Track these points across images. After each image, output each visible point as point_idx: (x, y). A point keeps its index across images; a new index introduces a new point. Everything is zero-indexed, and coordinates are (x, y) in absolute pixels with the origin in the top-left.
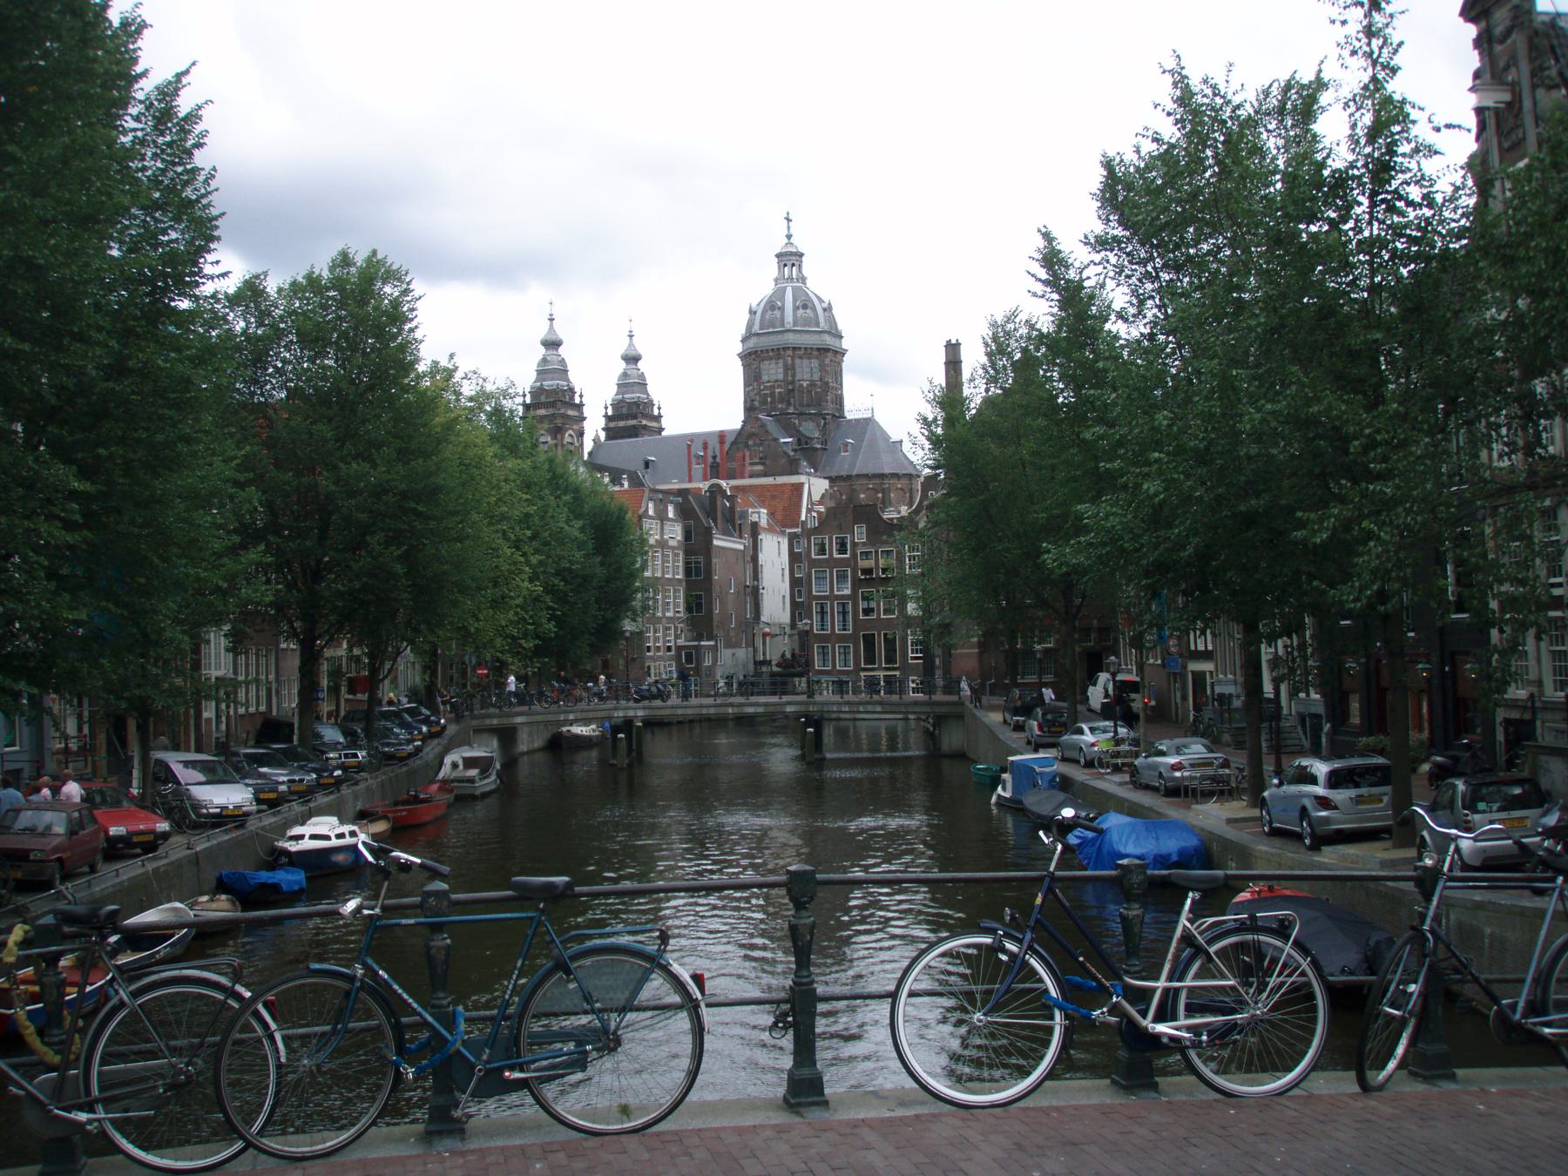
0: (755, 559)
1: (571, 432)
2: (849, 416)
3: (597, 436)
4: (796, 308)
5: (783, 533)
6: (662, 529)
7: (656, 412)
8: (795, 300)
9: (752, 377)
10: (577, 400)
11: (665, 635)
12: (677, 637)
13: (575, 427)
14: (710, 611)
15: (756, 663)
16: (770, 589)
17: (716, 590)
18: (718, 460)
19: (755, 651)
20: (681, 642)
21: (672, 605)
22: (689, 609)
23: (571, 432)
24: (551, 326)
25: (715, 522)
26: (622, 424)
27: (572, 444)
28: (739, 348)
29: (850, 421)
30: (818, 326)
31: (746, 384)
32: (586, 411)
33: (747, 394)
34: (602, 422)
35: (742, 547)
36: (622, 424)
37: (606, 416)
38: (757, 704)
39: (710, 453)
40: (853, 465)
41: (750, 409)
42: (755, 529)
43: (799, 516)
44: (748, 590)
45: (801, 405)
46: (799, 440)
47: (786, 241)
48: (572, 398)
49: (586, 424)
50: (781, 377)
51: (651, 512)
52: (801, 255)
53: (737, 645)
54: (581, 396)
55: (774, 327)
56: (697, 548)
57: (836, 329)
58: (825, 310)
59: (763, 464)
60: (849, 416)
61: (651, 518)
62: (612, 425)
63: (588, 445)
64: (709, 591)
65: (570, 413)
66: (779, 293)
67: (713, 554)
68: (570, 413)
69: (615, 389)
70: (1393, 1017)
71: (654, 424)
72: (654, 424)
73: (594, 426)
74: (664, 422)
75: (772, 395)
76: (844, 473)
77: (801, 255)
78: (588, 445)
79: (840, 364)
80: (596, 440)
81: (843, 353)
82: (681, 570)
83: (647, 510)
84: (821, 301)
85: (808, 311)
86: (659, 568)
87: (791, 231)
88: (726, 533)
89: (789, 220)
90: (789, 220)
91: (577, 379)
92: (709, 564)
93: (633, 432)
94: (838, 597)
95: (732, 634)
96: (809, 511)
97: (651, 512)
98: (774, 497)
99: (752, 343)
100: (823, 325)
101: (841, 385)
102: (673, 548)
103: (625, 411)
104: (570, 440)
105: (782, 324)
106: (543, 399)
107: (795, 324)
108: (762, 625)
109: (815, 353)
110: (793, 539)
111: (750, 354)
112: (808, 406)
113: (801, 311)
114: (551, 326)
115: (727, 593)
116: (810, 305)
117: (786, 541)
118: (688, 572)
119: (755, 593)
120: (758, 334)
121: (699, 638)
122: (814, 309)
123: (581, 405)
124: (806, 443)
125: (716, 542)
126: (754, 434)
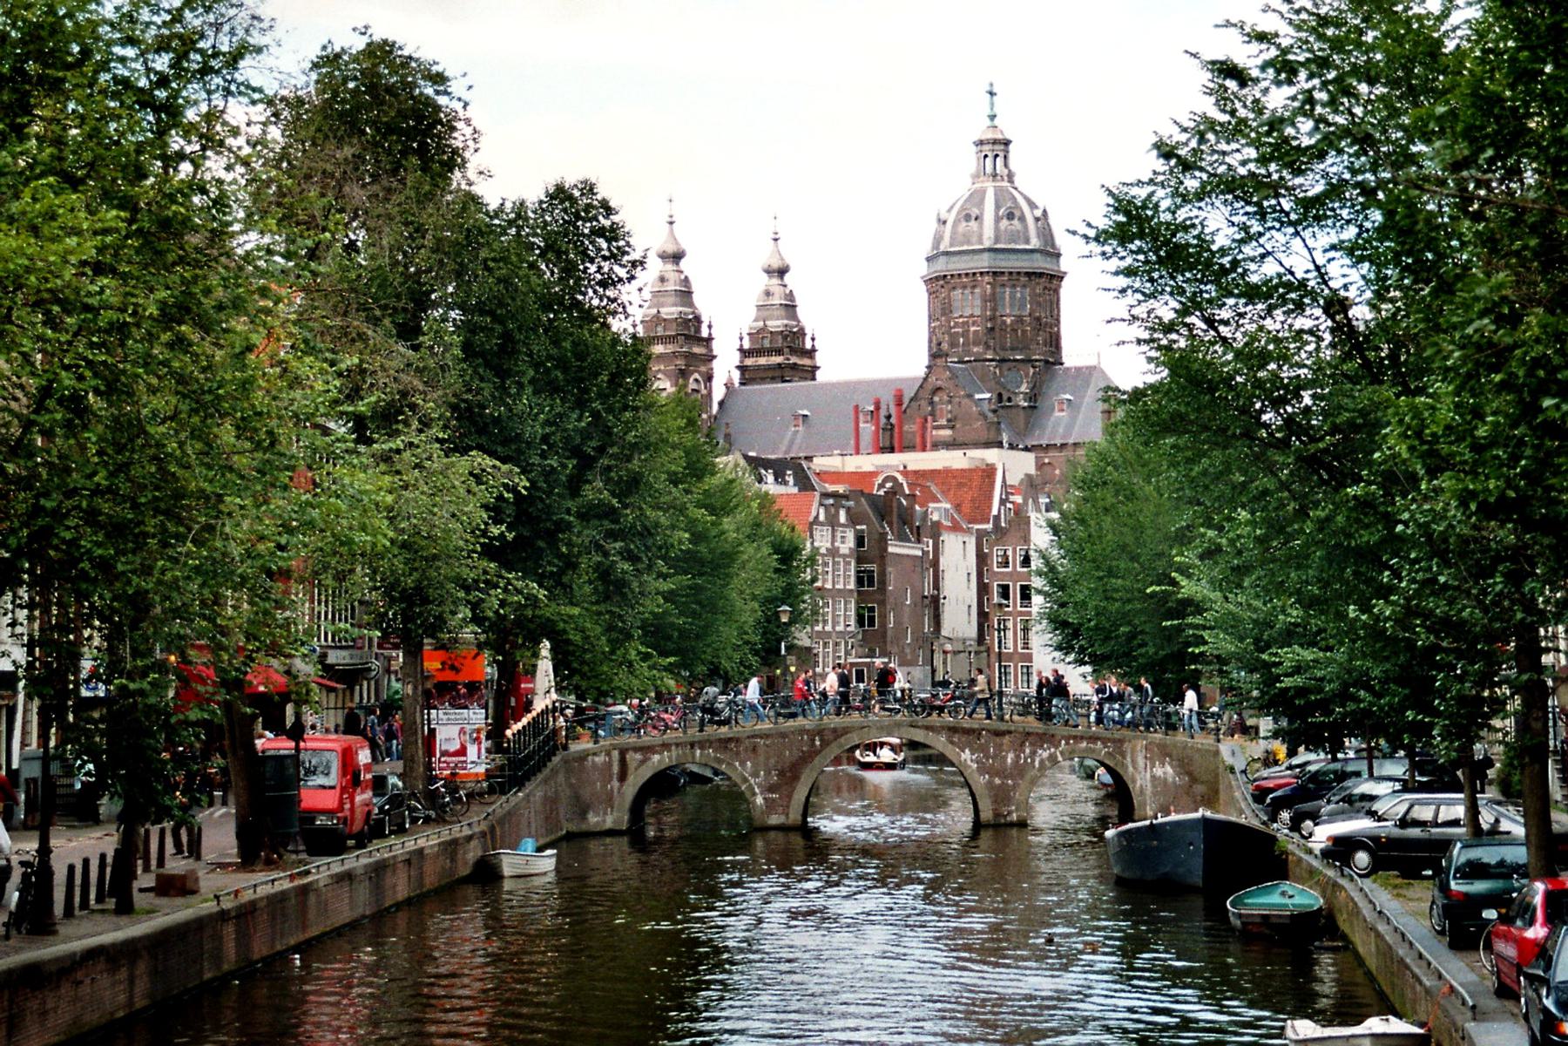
0: (935, 564)
1: (696, 376)
2: (1067, 364)
3: (730, 379)
4: (998, 219)
5: (969, 531)
6: (833, 536)
7: (808, 345)
8: (998, 207)
9: (940, 311)
10: (705, 333)
11: (835, 651)
12: (847, 653)
13: (703, 369)
14: (883, 625)
15: (935, 684)
16: (953, 602)
17: (891, 600)
18: (893, 420)
19: (934, 671)
20: (851, 660)
21: (841, 617)
22: (860, 620)
23: (696, 376)
24: (672, 231)
25: (890, 524)
26: (762, 361)
27: (697, 391)
28: (923, 269)
29: (1068, 369)
30: (1027, 241)
31: (931, 318)
32: (717, 347)
33: (932, 332)
34: (736, 358)
35: (919, 553)
36: (762, 361)
37: (741, 350)
38: (334, 970)
39: (883, 413)
40: (1070, 427)
41: (936, 355)
42: (936, 530)
43: (990, 507)
44: (927, 601)
45: (1004, 349)
46: (1000, 395)
47: (988, 123)
48: (698, 330)
49: (715, 364)
50: (977, 312)
51: (822, 518)
52: (1007, 143)
53: (913, 663)
54: (710, 327)
55: (969, 243)
56: (870, 556)
57: (1053, 245)
58: (1037, 219)
59: (953, 428)
60: (1067, 364)
61: (822, 524)
62: (749, 362)
63: (718, 393)
64: (882, 603)
65: (697, 350)
66: (977, 197)
67: (888, 560)
68: (697, 350)
69: (753, 312)
70: (779, 650)
71: (806, 362)
72: (806, 362)
73: (726, 367)
74: (819, 359)
75: (965, 334)
76: (1058, 442)
77: (1007, 143)
78: (718, 393)
79: (1056, 291)
80: (729, 386)
81: (1060, 277)
82: (853, 580)
83: (817, 517)
84: (1032, 205)
85: (1016, 222)
86: (830, 577)
87: (996, 110)
88: (902, 537)
89: (992, 94)
90: (992, 94)
91: (704, 303)
92: (883, 573)
93: (780, 374)
94: (1021, 614)
95: (908, 650)
96: (1003, 502)
97: (822, 518)
98: (960, 485)
99: (941, 266)
100: (1035, 243)
101: (1058, 320)
102: (844, 556)
103: (767, 344)
104: (695, 386)
105: (980, 241)
106: (660, 331)
107: (997, 240)
108: (942, 640)
109: (1023, 279)
110: (980, 536)
111: (937, 278)
112: (1012, 349)
113: (1004, 223)
114: (672, 231)
115: (903, 604)
116: (1017, 214)
117: (973, 540)
118: (860, 581)
119: (935, 604)
120: (947, 253)
121: (871, 654)
122: (1022, 219)
123: (710, 339)
124: (1009, 400)
125: (891, 549)
126: (939, 389)
